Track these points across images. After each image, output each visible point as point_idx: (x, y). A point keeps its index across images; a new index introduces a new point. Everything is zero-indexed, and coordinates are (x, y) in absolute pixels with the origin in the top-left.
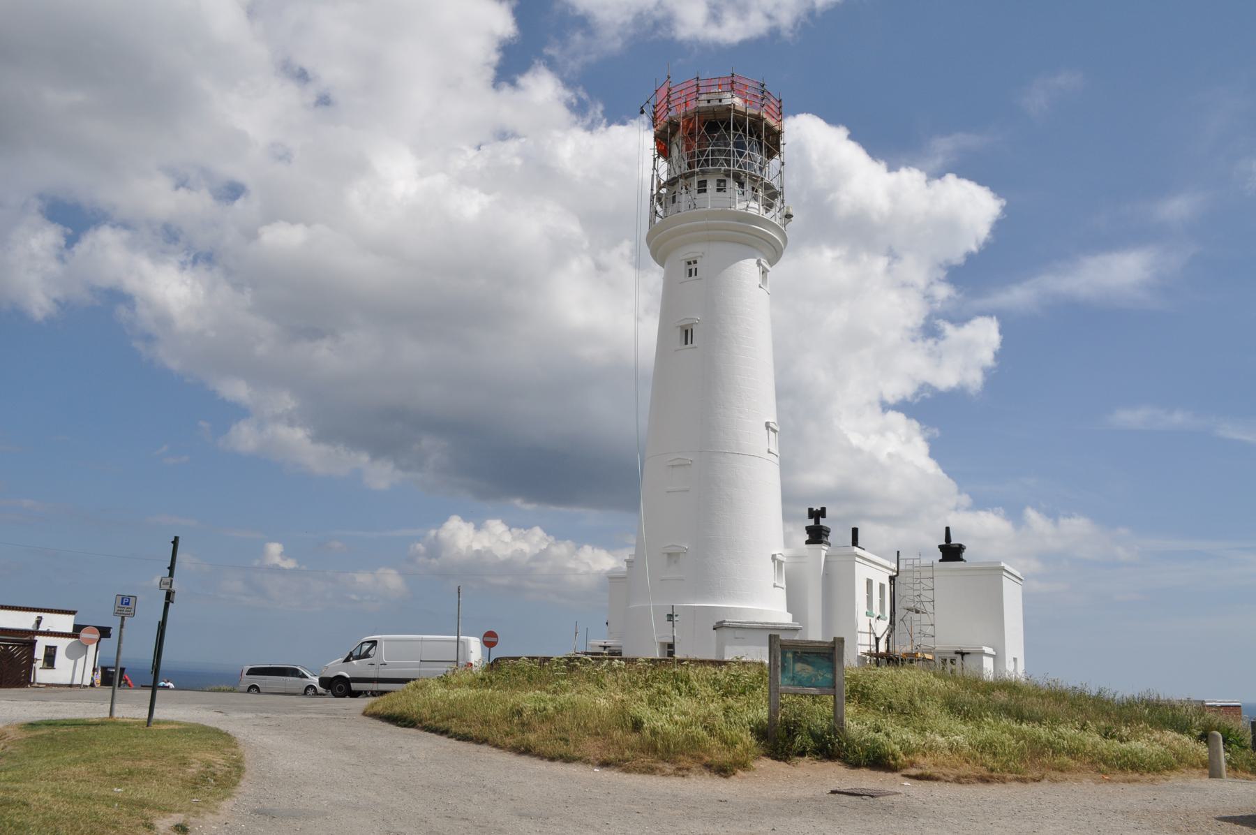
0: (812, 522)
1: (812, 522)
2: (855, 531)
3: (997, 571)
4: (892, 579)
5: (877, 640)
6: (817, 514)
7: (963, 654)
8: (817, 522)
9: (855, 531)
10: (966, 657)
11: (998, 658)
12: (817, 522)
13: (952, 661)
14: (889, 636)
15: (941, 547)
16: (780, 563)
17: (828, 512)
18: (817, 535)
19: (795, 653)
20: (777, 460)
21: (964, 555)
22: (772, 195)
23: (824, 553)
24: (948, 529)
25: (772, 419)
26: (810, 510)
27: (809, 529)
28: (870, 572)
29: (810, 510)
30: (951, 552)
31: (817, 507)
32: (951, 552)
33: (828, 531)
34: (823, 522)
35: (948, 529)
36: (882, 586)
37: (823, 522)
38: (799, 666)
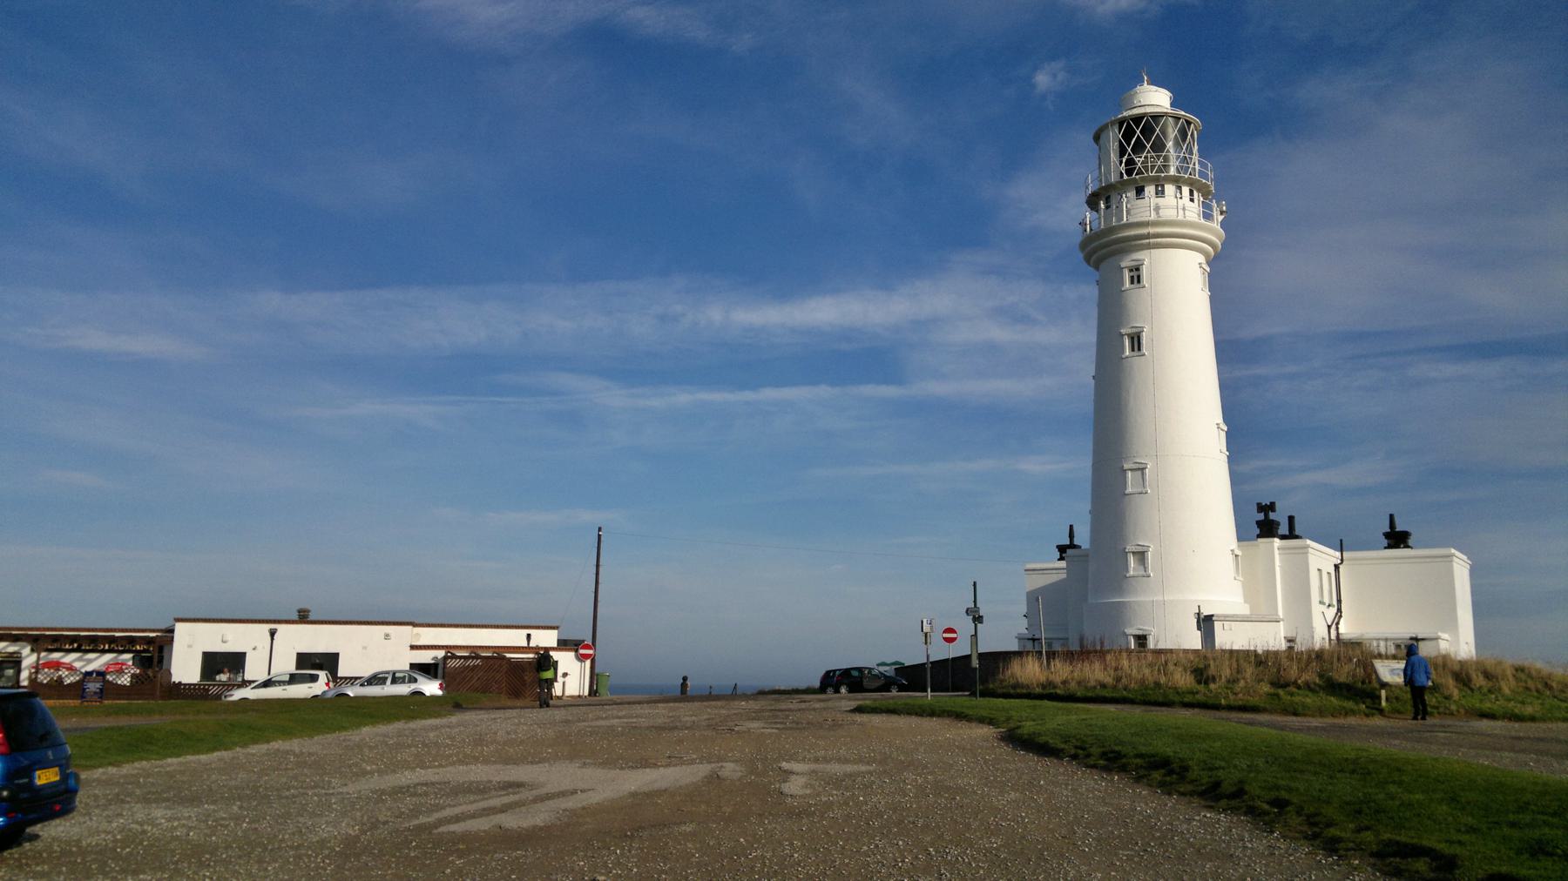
0: (1261, 516)
1: (1261, 516)
4: (1337, 567)
6: (1267, 508)
7: (1417, 639)
8: (1266, 515)
12: (1266, 515)
15: (1387, 535)
21: (1410, 542)
24: (1391, 517)
27: (1258, 523)
34: (1272, 516)
35: (1391, 517)
37: (1272, 516)
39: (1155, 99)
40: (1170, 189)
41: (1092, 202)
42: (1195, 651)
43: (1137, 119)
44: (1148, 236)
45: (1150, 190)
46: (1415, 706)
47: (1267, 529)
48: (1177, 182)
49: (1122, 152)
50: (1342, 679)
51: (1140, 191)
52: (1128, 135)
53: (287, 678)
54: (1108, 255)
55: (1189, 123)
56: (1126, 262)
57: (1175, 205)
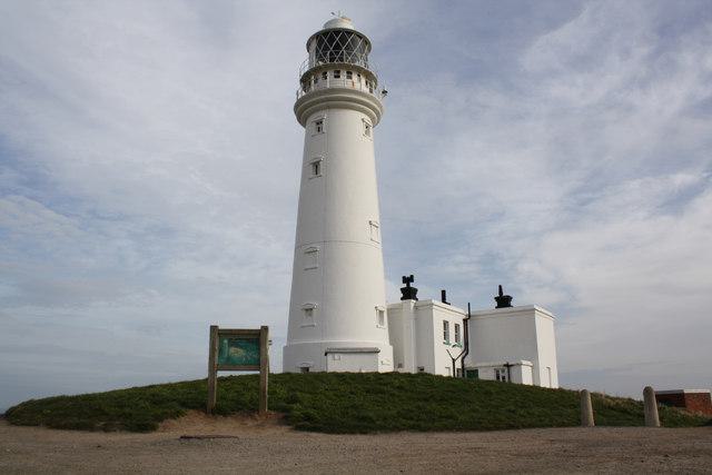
0: (405, 285)
1: (405, 285)
2: (444, 292)
3: (531, 311)
4: (465, 321)
5: (454, 361)
6: (408, 280)
7: (508, 366)
8: (408, 285)
9: (444, 292)
10: (512, 368)
11: (535, 369)
12: (408, 285)
13: (503, 371)
14: (463, 358)
16: (381, 312)
18: (409, 293)
19: (230, 340)
20: (380, 246)
21: (512, 303)
22: (370, 78)
23: (412, 305)
25: (376, 219)
26: (404, 277)
28: (448, 315)
29: (404, 277)
30: (503, 301)
31: (408, 276)
32: (503, 301)
33: (416, 290)
34: (412, 285)
36: (457, 326)
37: (412, 285)
38: (232, 350)
45: (343, 75)
49: (317, 52)
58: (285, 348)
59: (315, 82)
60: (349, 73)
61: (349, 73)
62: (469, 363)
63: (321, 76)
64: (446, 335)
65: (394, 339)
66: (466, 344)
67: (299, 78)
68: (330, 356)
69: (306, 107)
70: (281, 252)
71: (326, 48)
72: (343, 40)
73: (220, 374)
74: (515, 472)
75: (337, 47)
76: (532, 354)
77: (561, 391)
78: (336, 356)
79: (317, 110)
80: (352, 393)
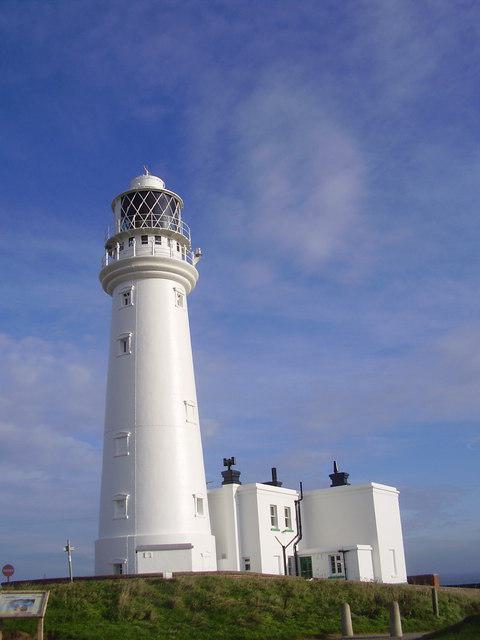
1: (226, 468)
2: (274, 471)
6: (229, 463)
7: (344, 552)
9: (274, 471)
13: (338, 558)
16: (200, 501)
17: (236, 461)
26: (225, 460)
31: (229, 457)
36: (287, 511)
37: (233, 468)
39: (155, 183)
40: (164, 240)
41: (110, 247)
42: (399, 587)
43: (144, 192)
44: (118, 274)
45: (151, 239)
46: (6, 584)
47: (230, 477)
48: (169, 235)
49: (123, 215)
50: (461, 619)
51: (144, 239)
52: (126, 204)
53: (247, 556)
54: (120, 280)
55: (177, 202)
56: (120, 289)
57: (165, 250)
58: (97, 543)
59: (122, 248)
60: (158, 238)
61: (158, 238)
62: (303, 552)
63: (126, 243)
64: (274, 521)
65: (216, 529)
66: (299, 527)
67: (98, 275)
68: (140, 554)
69: (113, 277)
70: (90, 458)
71: (132, 212)
72: (151, 201)
73: (400, 634)
74: (282, 637)
75: (144, 210)
76: (371, 536)
77: (218, 572)
78: (147, 553)
79: (120, 282)
80: (302, 598)
